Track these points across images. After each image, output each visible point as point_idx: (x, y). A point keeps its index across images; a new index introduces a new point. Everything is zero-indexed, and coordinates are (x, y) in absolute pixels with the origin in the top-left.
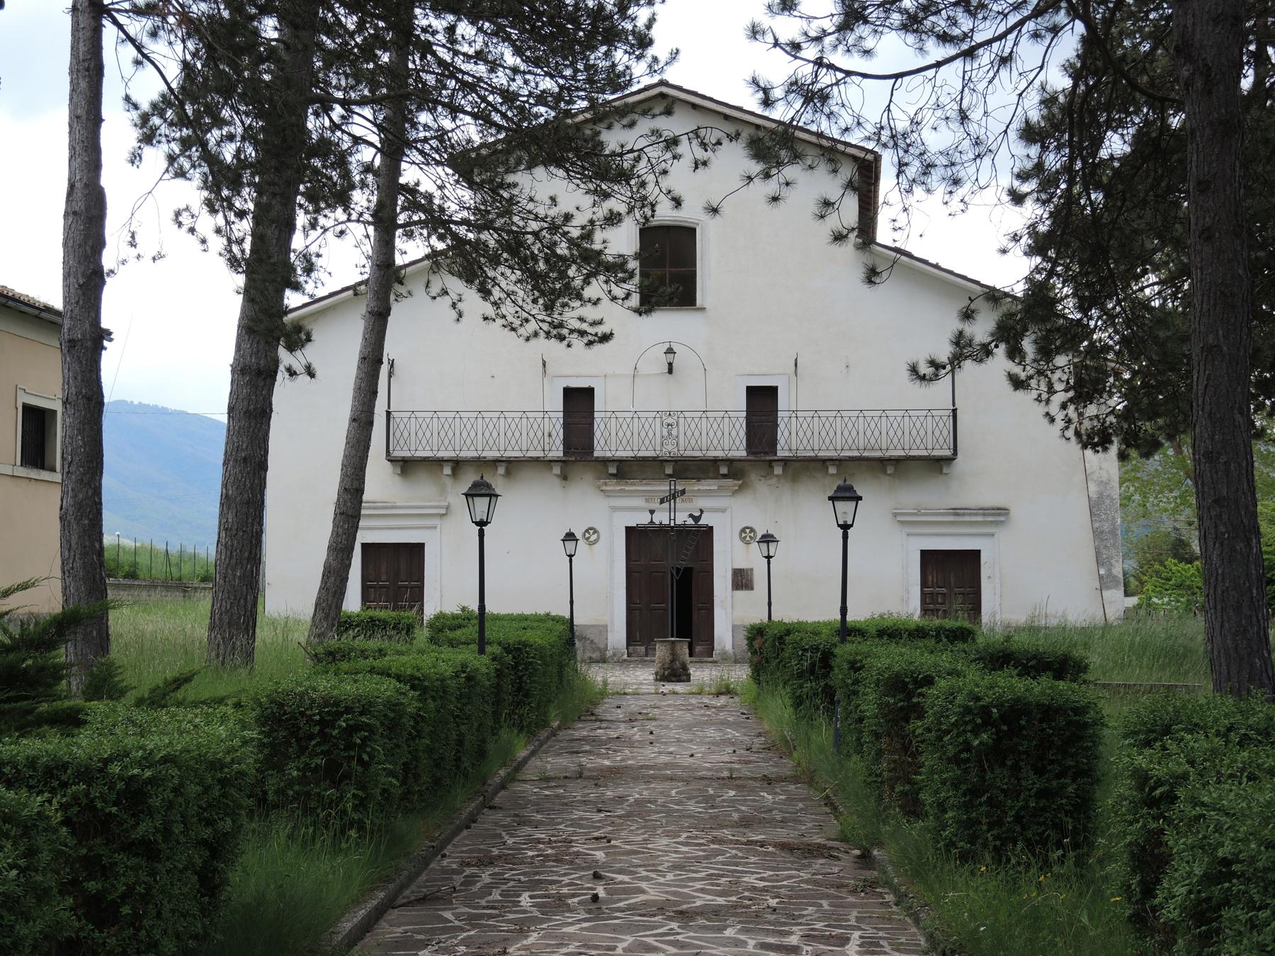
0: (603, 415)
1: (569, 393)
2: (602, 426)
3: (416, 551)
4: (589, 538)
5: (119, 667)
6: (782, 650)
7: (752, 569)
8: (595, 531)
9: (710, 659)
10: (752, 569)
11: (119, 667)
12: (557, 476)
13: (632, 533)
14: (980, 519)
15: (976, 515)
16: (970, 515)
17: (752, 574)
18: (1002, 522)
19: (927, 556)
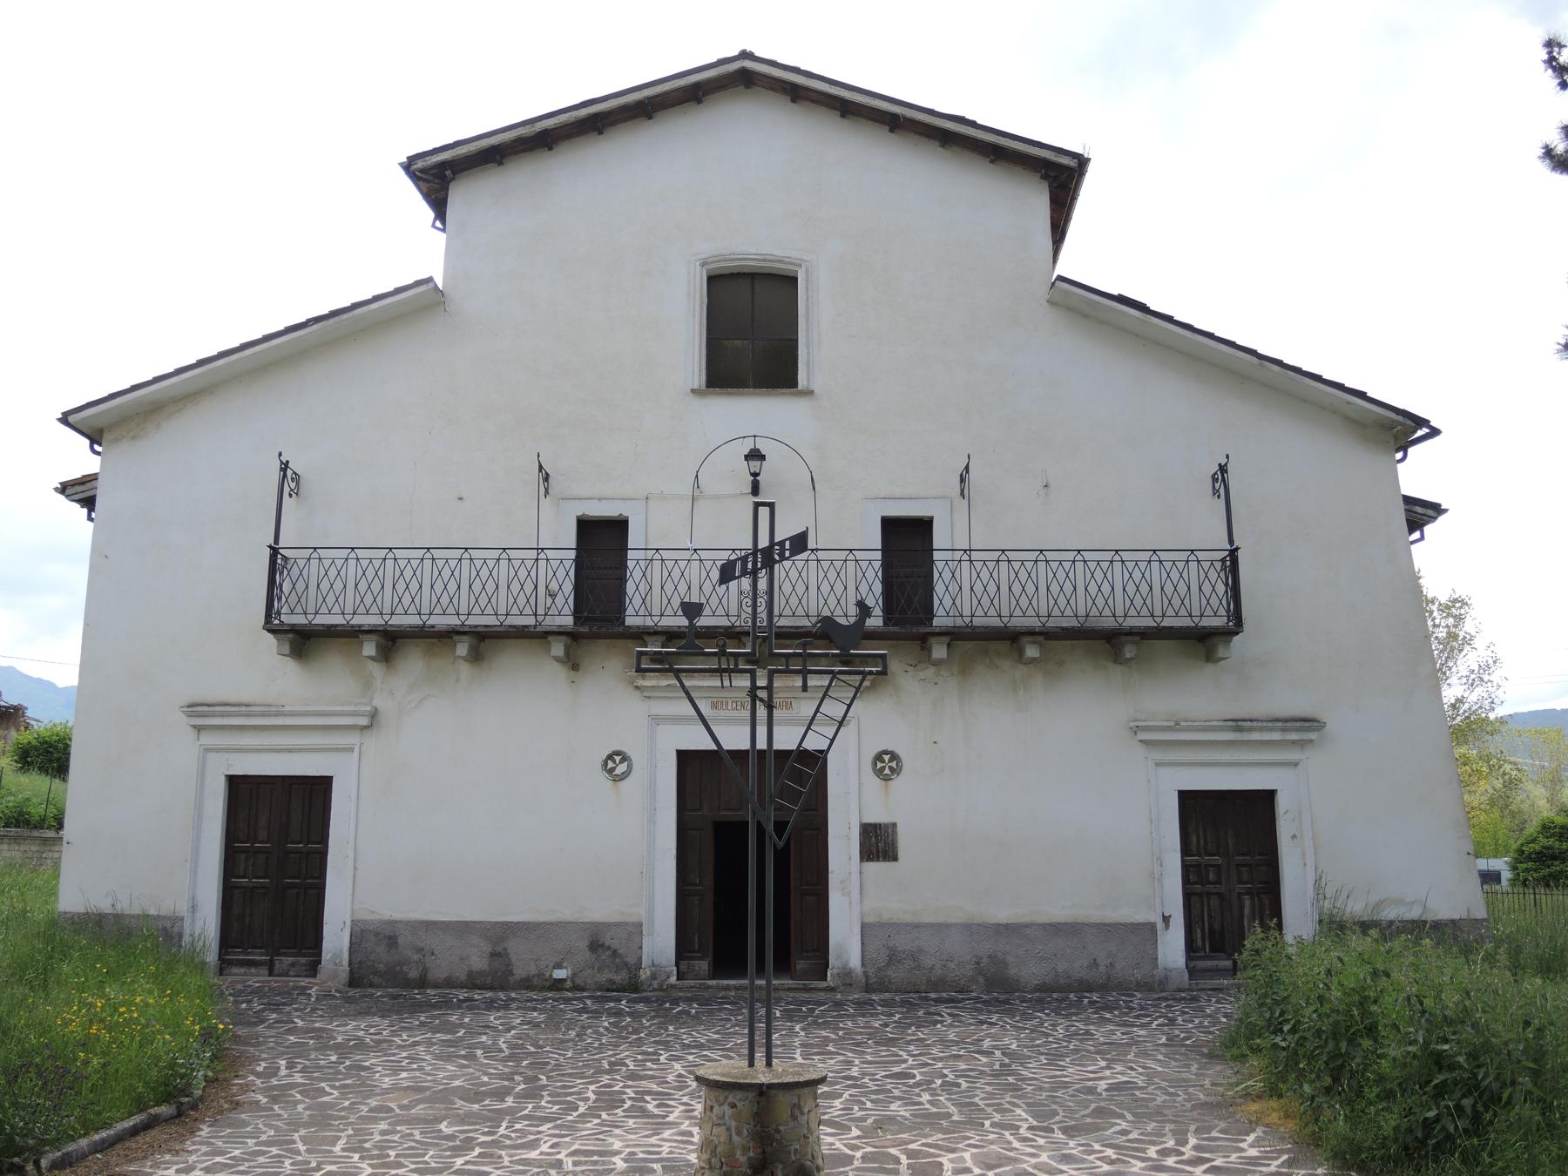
0: (948, 555)
1: (587, 527)
2: (947, 575)
3: (317, 790)
4: (613, 769)
7: (894, 825)
8: (625, 758)
9: (823, 984)
10: (894, 825)
12: (557, 659)
13: (687, 760)
14: (1276, 736)
15: (1271, 729)
16: (1261, 729)
17: (895, 833)
18: (1311, 741)
19: (1190, 802)
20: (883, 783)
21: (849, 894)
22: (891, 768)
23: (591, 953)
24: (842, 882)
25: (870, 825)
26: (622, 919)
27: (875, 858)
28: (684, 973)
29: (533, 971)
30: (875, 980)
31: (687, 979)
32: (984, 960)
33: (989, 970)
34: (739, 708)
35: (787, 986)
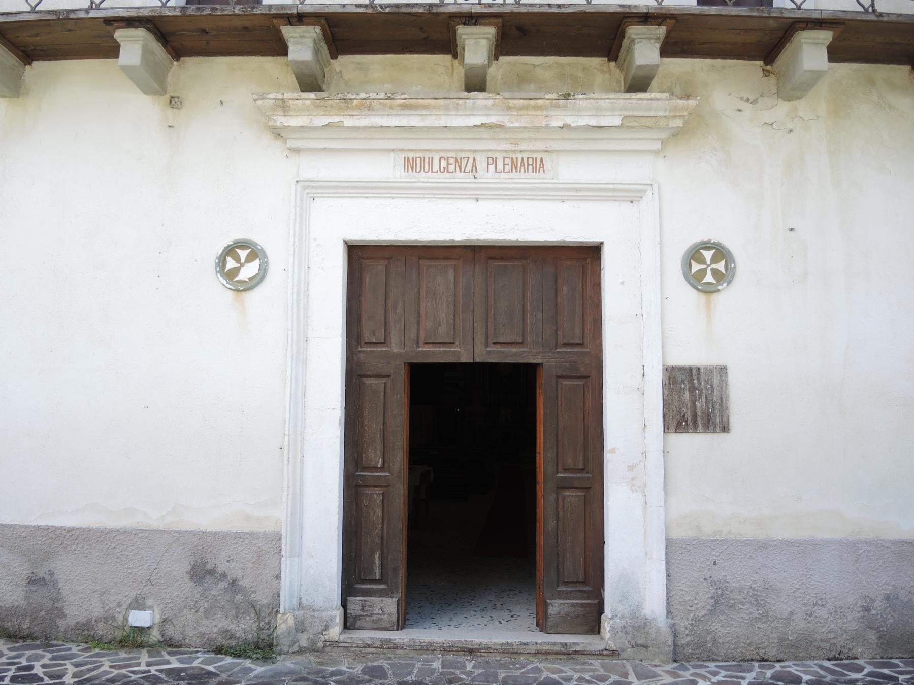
4: (235, 271)
5: (34, 633)
6: (648, 633)
7: (723, 370)
8: (255, 253)
10: (723, 370)
11: (34, 633)
20: (703, 297)
21: (643, 489)
22: (715, 273)
23: (193, 584)
24: (631, 468)
25: (681, 369)
26: (247, 527)
27: (691, 426)
28: (356, 618)
29: (97, 611)
30: (688, 639)
31: (360, 628)
32: (877, 604)
33: (884, 621)
34: (452, 168)
35: (534, 647)
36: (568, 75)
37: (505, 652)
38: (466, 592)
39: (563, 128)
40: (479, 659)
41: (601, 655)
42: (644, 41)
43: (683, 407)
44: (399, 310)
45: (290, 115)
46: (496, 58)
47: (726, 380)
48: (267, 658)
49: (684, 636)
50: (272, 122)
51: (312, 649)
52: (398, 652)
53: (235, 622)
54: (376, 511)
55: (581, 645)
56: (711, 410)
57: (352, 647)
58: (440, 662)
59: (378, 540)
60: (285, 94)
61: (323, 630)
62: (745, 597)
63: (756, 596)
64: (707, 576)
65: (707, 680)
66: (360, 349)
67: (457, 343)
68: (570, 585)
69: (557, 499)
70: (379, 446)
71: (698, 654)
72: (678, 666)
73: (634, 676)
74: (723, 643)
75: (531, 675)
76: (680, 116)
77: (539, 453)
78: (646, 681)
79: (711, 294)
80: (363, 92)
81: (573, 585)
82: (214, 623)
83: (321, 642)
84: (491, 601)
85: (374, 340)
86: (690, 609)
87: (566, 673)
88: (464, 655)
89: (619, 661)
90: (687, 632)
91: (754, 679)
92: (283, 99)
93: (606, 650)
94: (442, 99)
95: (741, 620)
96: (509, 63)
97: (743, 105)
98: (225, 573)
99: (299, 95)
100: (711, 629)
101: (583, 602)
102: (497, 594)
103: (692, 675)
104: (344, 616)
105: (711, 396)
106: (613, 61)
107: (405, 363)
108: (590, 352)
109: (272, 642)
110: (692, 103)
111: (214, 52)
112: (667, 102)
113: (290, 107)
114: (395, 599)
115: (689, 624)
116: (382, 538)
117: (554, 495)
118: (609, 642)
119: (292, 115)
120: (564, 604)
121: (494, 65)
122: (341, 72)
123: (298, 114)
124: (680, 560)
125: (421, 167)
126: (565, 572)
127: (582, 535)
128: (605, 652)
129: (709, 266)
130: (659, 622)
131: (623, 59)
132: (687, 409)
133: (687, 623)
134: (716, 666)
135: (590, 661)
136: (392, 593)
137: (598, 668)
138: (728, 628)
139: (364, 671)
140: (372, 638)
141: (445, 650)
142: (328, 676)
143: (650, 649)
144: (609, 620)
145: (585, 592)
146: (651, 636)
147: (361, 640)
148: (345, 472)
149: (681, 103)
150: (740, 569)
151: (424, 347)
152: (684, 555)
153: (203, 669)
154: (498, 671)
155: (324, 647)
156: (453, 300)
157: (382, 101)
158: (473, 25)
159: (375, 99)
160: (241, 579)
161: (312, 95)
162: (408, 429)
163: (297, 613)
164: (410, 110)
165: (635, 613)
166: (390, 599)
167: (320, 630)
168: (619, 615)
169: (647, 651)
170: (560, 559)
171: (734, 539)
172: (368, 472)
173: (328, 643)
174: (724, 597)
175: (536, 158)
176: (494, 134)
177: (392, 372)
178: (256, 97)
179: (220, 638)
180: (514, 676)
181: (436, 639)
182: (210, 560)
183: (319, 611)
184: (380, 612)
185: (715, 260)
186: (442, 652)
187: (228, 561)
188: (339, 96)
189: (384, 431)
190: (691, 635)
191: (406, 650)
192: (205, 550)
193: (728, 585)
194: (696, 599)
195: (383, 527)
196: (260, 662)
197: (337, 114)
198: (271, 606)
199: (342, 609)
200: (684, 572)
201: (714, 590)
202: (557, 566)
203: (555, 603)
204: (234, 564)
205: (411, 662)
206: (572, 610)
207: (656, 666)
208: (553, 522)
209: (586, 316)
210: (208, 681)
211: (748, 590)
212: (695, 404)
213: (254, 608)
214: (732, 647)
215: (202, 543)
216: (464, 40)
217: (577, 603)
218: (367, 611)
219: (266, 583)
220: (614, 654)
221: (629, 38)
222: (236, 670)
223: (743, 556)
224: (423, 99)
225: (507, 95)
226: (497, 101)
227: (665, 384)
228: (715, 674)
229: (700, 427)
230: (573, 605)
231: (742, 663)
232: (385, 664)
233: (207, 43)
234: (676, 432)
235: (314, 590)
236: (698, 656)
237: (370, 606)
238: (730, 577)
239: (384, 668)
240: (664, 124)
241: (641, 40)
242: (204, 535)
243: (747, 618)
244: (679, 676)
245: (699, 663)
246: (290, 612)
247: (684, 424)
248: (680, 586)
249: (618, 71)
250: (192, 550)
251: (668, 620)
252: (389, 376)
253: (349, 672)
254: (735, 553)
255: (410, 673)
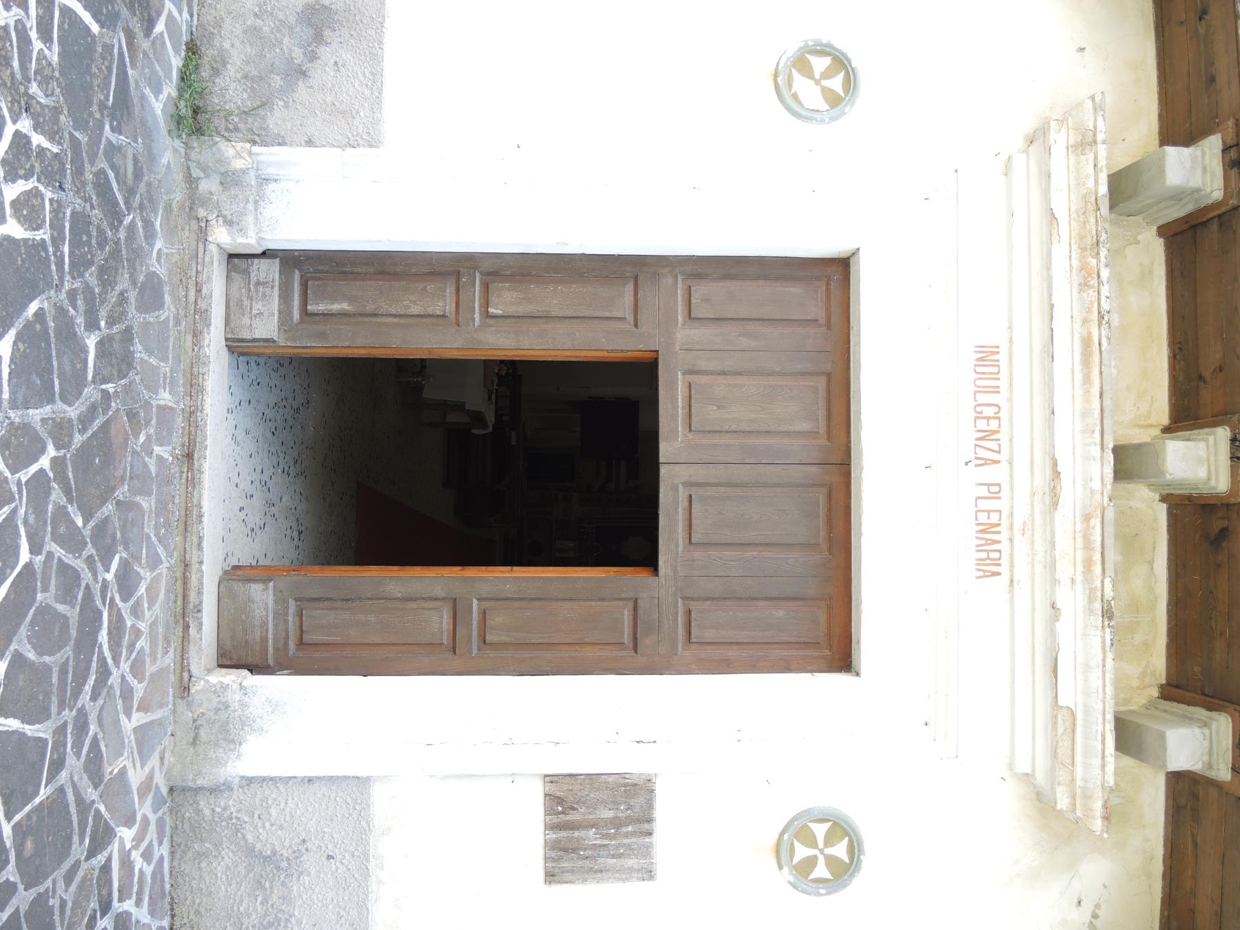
4: (806, 70)
6: (217, 745)
7: (648, 874)
10: (648, 874)
17: (626, 874)
22: (810, 863)
25: (650, 804)
27: (555, 820)
28: (246, 272)
30: (207, 812)
34: (982, 424)
35: (195, 559)
36: (1137, 617)
37: (188, 512)
38: (296, 462)
39: (1053, 608)
40: (174, 470)
41: (182, 668)
42: (1206, 743)
43: (587, 808)
44: (744, 342)
45: (1068, 155)
46: (1164, 499)
47: (633, 880)
48: (178, 123)
49: (211, 805)
50: (1057, 127)
51: (194, 200)
52: (189, 338)
53: (239, 76)
54: (417, 305)
55: (198, 636)
56: (582, 853)
57: (197, 264)
58: (170, 404)
59: (370, 308)
60: (1105, 146)
61: (224, 217)
62: (275, 906)
63: (276, 924)
64: (309, 845)
65: (134, 843)
66: (680, 278)
67: (690, 436)
68: (297, 619)
69: (436, 599)
70: (521, 309)
71: (183, 828)
72: (162, 795)
73: (143, 721)
74: (200, 869)
75: (144, 552)
76: (1075, 805)
77: (512, 570)
78: (133, 742)
79: (774, 854)
80: (1110, 273)
81: (298, 625)
82: (237, 43)
83: (205, 214)
84: (281, 499)
85: (696, 301)
86: (256, 816)
87: (149, 609)
88: (183, 445)
89: (171, 698)
90: (218, 810)
91: (138, 922)
92: (1095, 142)
93: (191, 676)
94: (1102, 405)
95: (237, 898)
96: (1155, 520)
97: (1088, 908)
98: (316, 58)
99: (1104, 169)
100: (223, 849)
101: (270, 641)
102: (293, 510)
103: (145, 819)
104: (248, 255)
105: (605, 853)
106: (1161, 693)
107: (657, 351)
108: (676, 655)
109: (207, 133)
110: (1098, 825)
111: (1163, 36)
112: (1099, 783)
113: (1082, 154)
114: (274, 335)
115: (232, 813)
116: (374, 315)
117: (442, 595)
118: (202, 682)
119: (1068, 159)
120: (266, 608)
121: (1152, 494)
122: (1138, 242)
123: (1071, 170)
124: (335, 800)
125: (984, 373)
126: (318, 612)
127: (378, 640)
128: (186, 675)
129: (822, 851)
130: (234, 764)
131: (1168, 708)
132: (584, 814)
133: (233, 810)
134: (162, 858)
135: (171, 652)
136: (285, 330)
137: (158, 663)
138: (224, 878)
139: (152, 276)
140: (211, 296)
141: (191, 413)
142: (144, 214)
143: (192, 749)
144: (239, 681)
145: (286, 644)
146: (212, 750)
147: (209, 279)
148: (481, 255)
149: (1098, 806)
150: (320, 898)
151: (683, 381)
152: (344, 807)
153: (159, 15)
154: (153, 496)
155: (198, 219)
156: (761, 429)
157: (1096, 305)
158: (1231, 453)
159: (1099, 294)
160: (308, 84)
161: (1103, 189)
162: (550, 359)
163: (252, 173)
164: (1082, 354)
165: (250, 725)
166: (276, 327)
167: (225, 213)
168: (247, 699)
169: (187, 744)
170: (339, 604)
171: (370, 890)
172: (480, 291)
173: (203, 225)
174: (275, 872)
175: (1000, 565)
176: (1041, 493)
177: (643, 330)
178: (1098, 99)
179: (211, 52)
180: (143, 524)
181: (209, 399)
182: (338, 35)
183: (256, 210)
184: (255, 312)
185: (832, 861)
186: (188, 409)
187: (336, 63)
188: (1103, 234)
189: (547, 318)
190: (214, 817)
191: (191, 350)
192: (354, 26)
193: (294, 879)
194: (272, 825)
195: (391, 315)
196: (172, 110)
197: (1072, 233)
198: (263, 133)
199: (259, 251)
200: (316, 806)
201: (286, 855)
202: (328, 599)
203: (267, 594)
204: (332, 73)
205: (170, 356)
206: (257, 622)
207: (162, 759)
208: (400, 592)
209: (735, 647)
210: (135, 15)
211: (286, 911)
212: (592, 826)
213: (261, 106)
214: (194, 884)
215: (365, 21)
216: (1206, 441)
217: (267, 631)
218: (257, 291)
219: (301, 125)
220: (184, 689)
221: (1211, 718)
222: (158, 68)
223: (341, 904)
224: (1101, 373)
225: (1110, 514)
226: (1098, 497)
227: (625, 778)
228: (147, 856)
229: (554, 836)
230: (264, 624)
231: (168, 899)
232: (166, 314)
233: (1182, 23)
234: (546, 795)
235: (288, 203)
236: (180, 827)
237: (264, 295)
238: (307, 882)
239: (159, 310)
240: (1061, 779)
241: (1208, 738)
242: (378, 25)
243: (241, 909)
244: (142, 795)
245: (168, 829)
246: (253, 163)
247: (560, 808)
248: (293, 799)
249: (1144, 702)
250: (354, 5)
251: (237, 779)
252: (636, 326)
253: (152, 251)
254: (347, 892)
255: (148, 350)
